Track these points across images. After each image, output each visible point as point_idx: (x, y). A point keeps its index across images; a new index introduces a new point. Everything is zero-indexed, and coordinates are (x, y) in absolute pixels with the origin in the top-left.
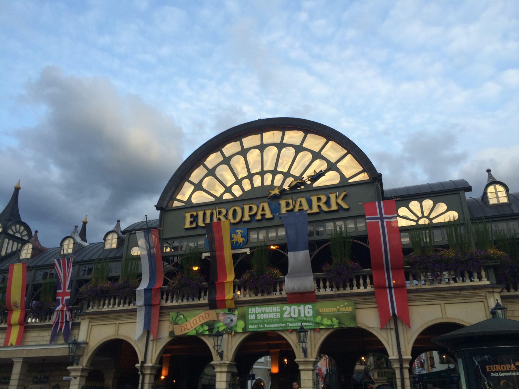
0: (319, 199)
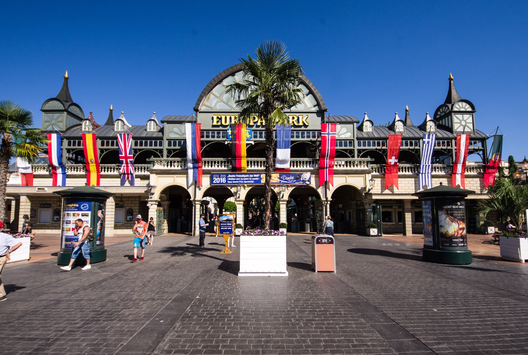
0: (293, 118)
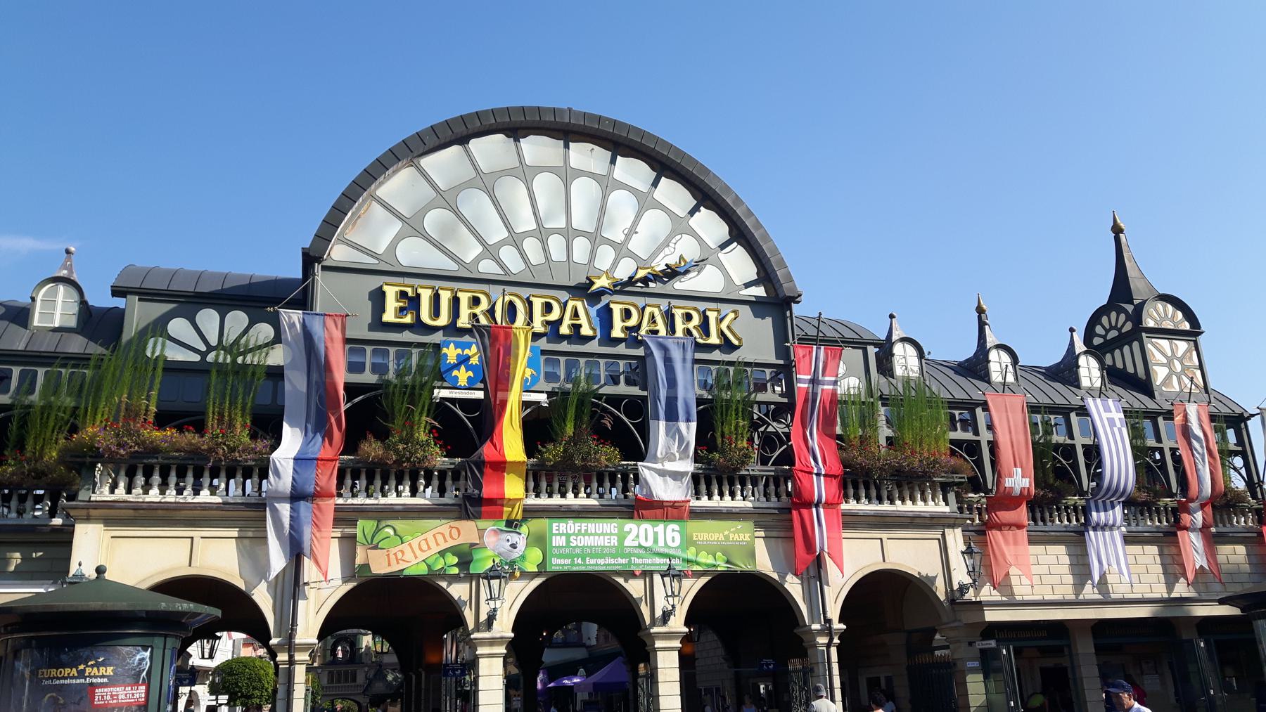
0: (476, 301)
